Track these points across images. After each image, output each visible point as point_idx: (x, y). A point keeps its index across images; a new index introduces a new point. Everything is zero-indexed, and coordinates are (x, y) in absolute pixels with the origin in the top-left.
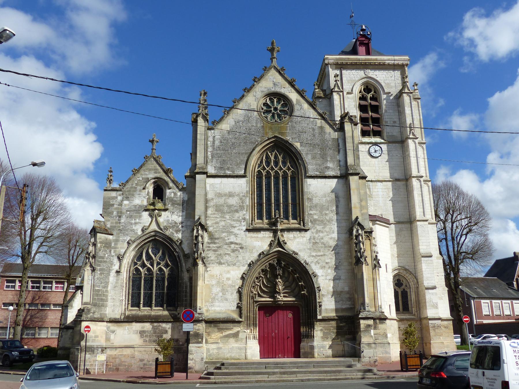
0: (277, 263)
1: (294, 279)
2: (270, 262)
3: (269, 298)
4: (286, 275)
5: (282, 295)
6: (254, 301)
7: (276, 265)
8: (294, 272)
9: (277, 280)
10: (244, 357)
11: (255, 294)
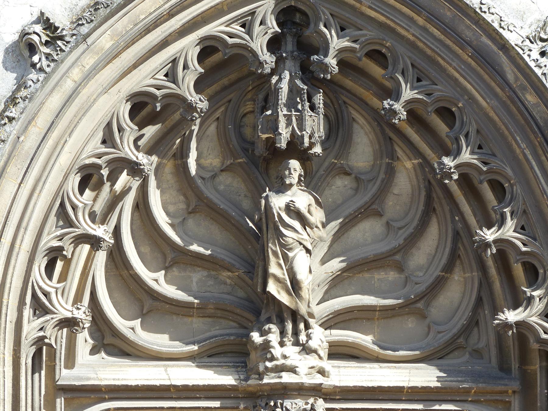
0: (274, 44)
1: (433, 193)
2: (214, 28)
3: (201, 359)
4: (363, 151)
5: (320, 338)
6: (57, 390)
7: (268, 59)
8: (438, 121)
9: (278, 202)
10: (74, 83)
11: (70, 324)
